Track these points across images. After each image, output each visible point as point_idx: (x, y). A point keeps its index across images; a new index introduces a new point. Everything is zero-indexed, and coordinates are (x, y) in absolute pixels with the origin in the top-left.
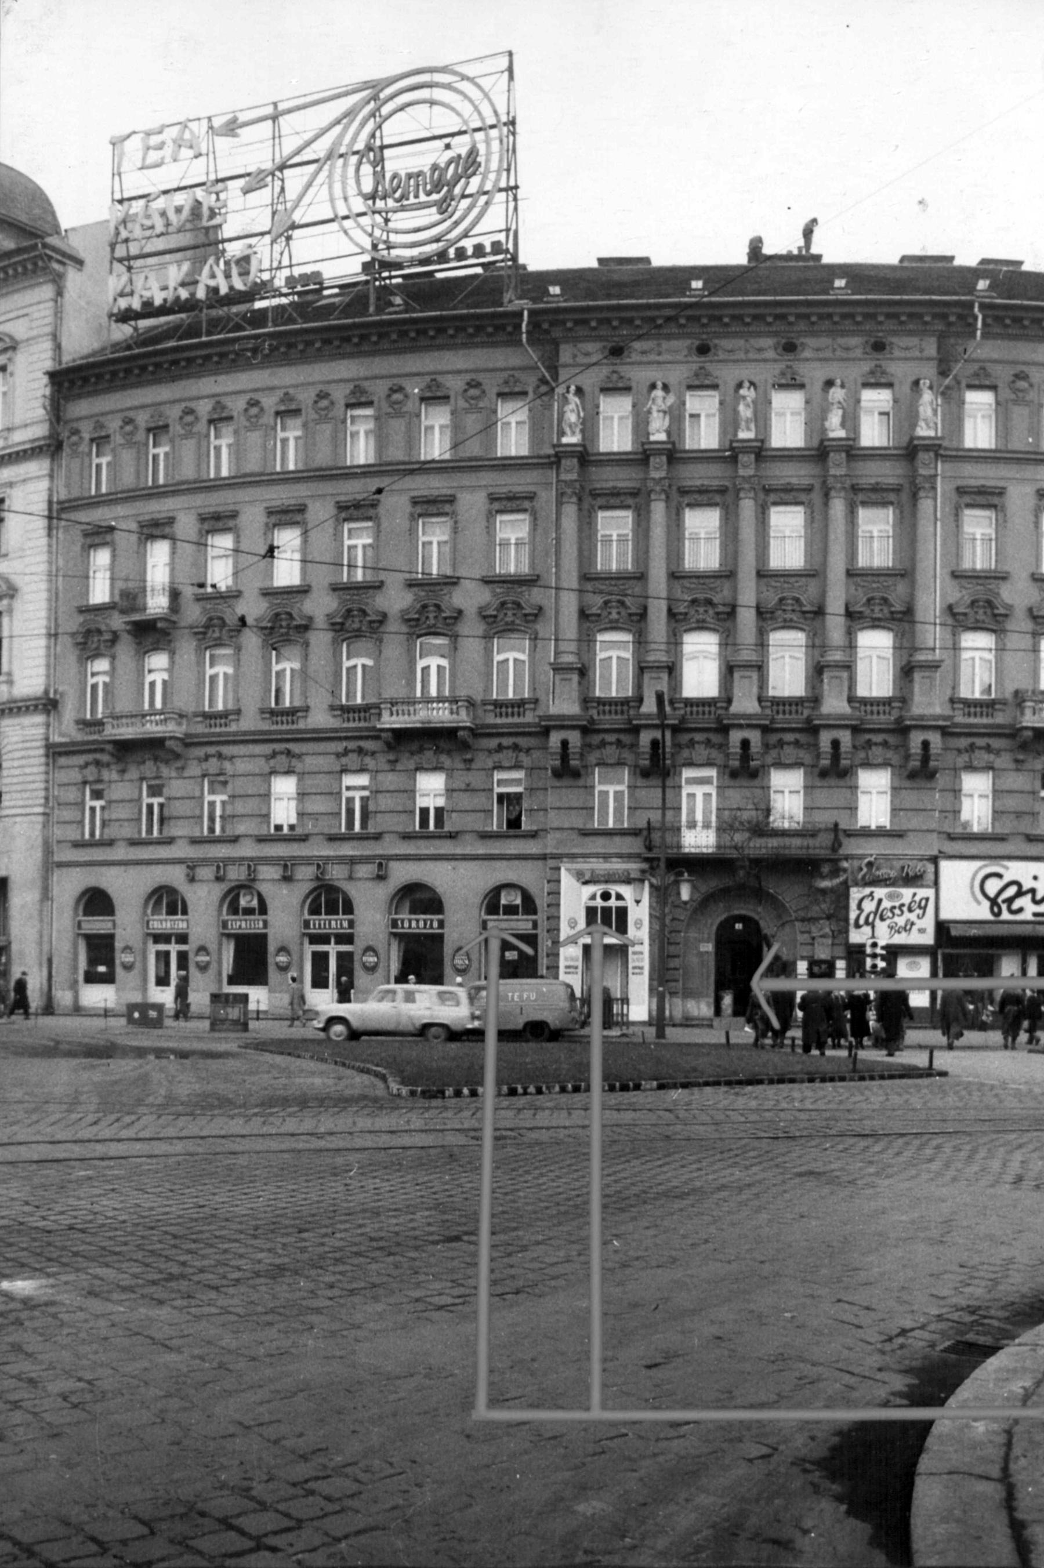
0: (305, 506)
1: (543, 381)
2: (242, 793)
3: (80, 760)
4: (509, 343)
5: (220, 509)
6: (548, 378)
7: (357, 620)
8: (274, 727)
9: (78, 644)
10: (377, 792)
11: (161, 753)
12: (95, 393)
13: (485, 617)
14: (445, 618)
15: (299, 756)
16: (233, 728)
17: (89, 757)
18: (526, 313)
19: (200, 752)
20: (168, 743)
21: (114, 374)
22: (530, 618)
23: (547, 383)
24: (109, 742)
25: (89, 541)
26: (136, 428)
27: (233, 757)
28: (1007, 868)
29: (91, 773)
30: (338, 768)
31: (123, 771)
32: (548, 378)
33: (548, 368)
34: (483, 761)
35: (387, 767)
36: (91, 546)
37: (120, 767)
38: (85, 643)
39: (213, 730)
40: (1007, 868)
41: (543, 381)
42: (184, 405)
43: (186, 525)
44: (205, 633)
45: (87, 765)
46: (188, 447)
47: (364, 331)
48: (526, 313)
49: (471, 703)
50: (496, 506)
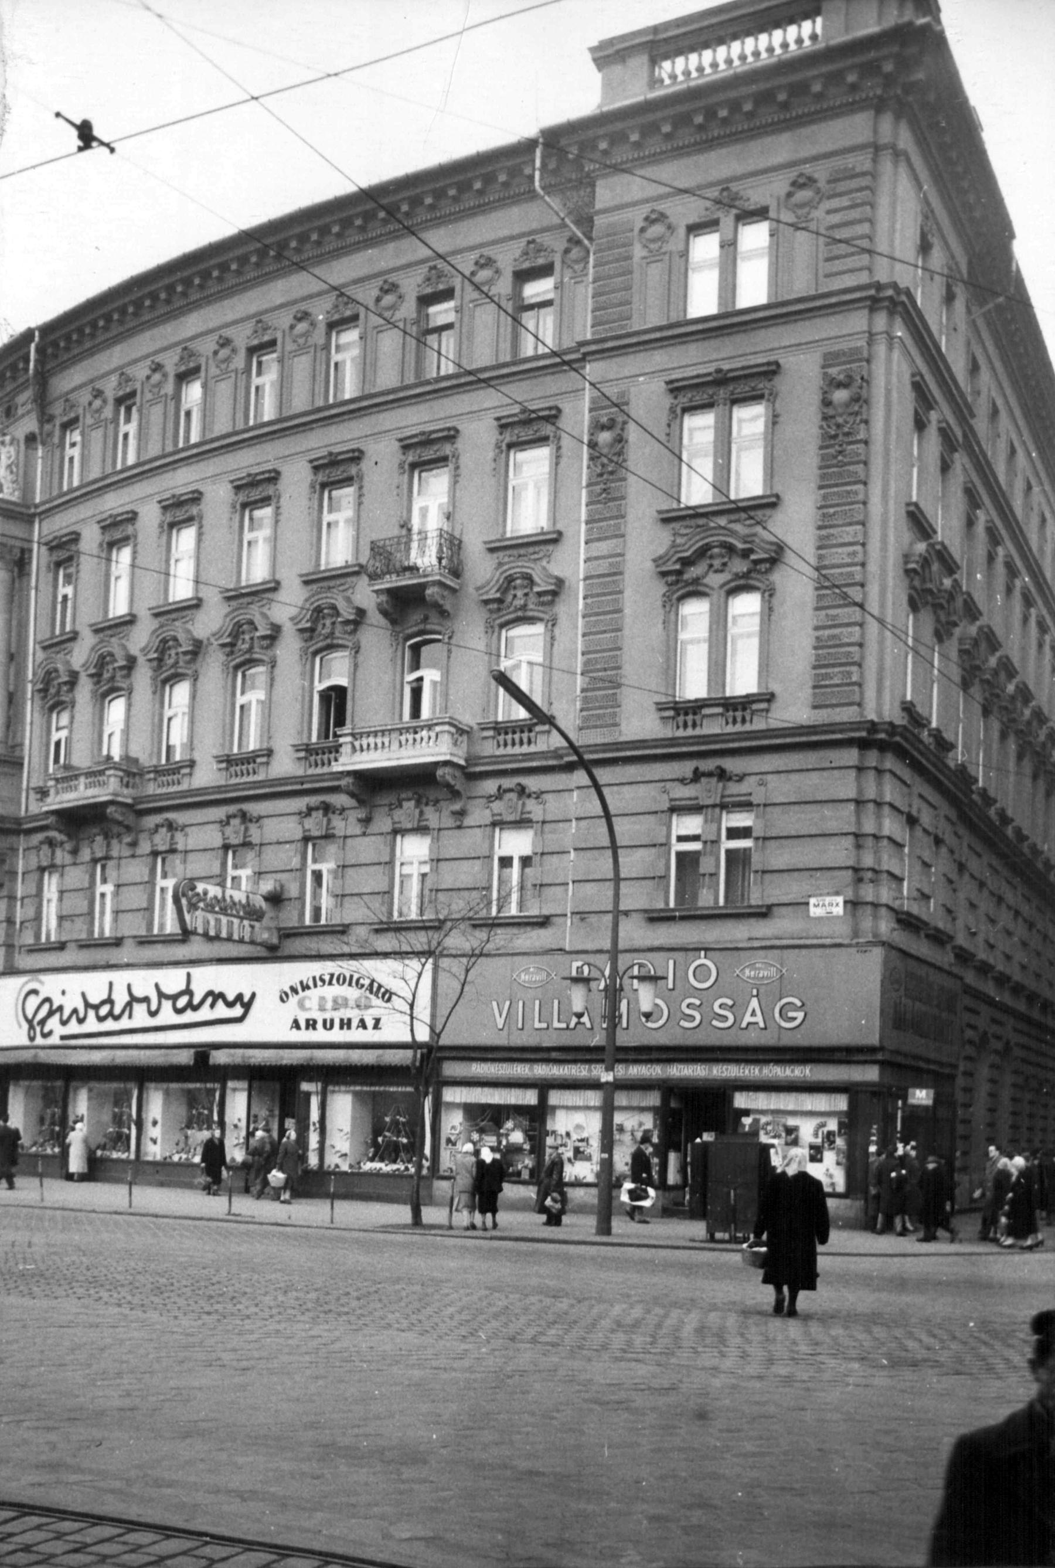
0: (278, 473)
1: (574, 241)
2: (353, 862)
3: (300, 804)
4: (516, 199)
5: (255, 470)
6: (580, 235)
7: (520, 593)
8: (730, 729)
9: (302, 631)
10: (438, 860)
11: (432, 794)
12: (208, 300)
13: (664, 574)
14: (540, 594)
15: (538, 795)
16: (759, 724)
17: (314, 800)
18: (37, 334)
19: (490, 786)
20: (440, 772)
21: (138, 304)
22: (763, 567)
23: (578, 242)
24: (349, 773)
25: (321, 477)
26: (313, 324)
27: (259, 818)
28: (42, 983)
29: (314, 825)
30: (666, 805)
31: (367, 821)
32: (580, 235)
33: (577, 223)
34: (479, 814)
35: (358, 830)
36: (510, 446)
37: (361, 814)
38: (232, 645)
39: (510, 750)
40: (42, 983)
41: (574, 241)
42: (294, 309)
43: (150, 516)
44: (679, 573)
45: (310, 810)
46: (302, 365)
47: (460, 178)
48: (37, 334)
49: (461, 731)
50: (684, 400)
